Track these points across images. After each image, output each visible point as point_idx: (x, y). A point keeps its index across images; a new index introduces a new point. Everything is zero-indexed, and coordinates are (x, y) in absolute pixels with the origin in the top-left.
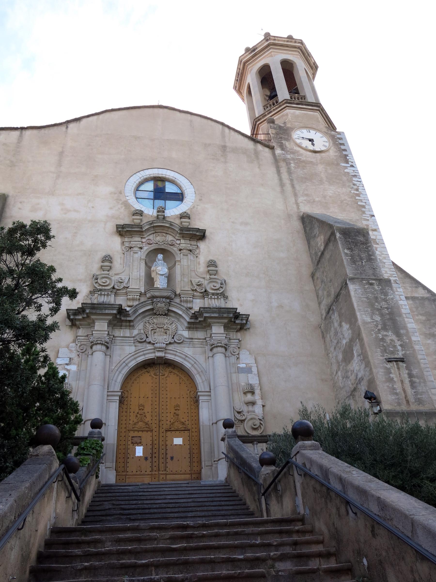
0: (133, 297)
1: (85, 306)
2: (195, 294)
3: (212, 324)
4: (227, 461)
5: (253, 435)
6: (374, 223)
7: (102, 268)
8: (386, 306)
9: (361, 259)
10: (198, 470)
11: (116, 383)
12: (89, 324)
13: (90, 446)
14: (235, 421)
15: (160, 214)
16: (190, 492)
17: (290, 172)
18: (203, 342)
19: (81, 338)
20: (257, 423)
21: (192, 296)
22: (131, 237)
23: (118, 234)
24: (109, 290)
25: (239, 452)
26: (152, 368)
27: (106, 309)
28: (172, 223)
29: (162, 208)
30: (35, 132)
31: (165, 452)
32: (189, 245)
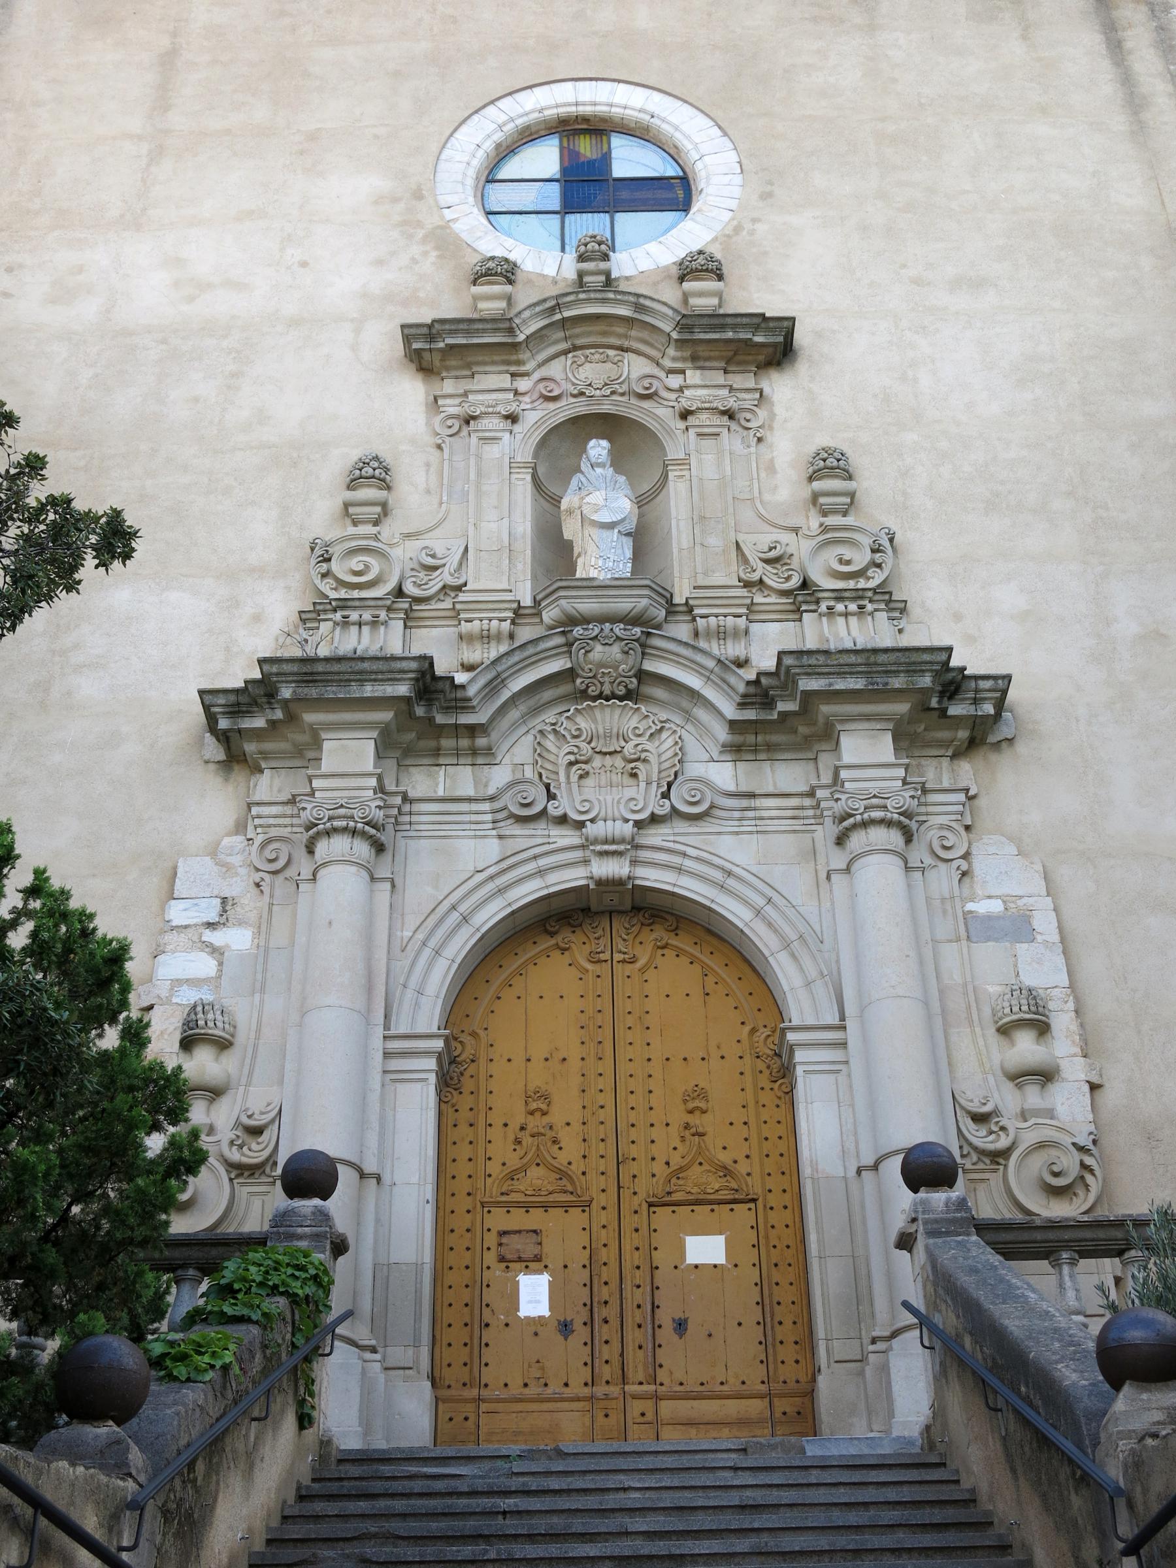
0: (485, 627)
1: (275, 669)
2: (759, 599)
3: (839, 727)
4: (931, 1348)
5: (1050, 1221)
7: (347, 513)
10: (803, 1379)
11: (423, 1000)
12: (299, 752)
13: (259, 1279)
14: (963, 1156)
16: (751, 1496)
18: (802, 808)
19: (266, 810)
20: (1070, 1162)
21: (744, 610)
22: (469, 373)
23: (413, 367)
24: (380, 603)
25: (987, 1305)
26: (578, 930)
27: (363, 677)
28: (642, 301)
31: (649, 1299)
32: (725, 392)
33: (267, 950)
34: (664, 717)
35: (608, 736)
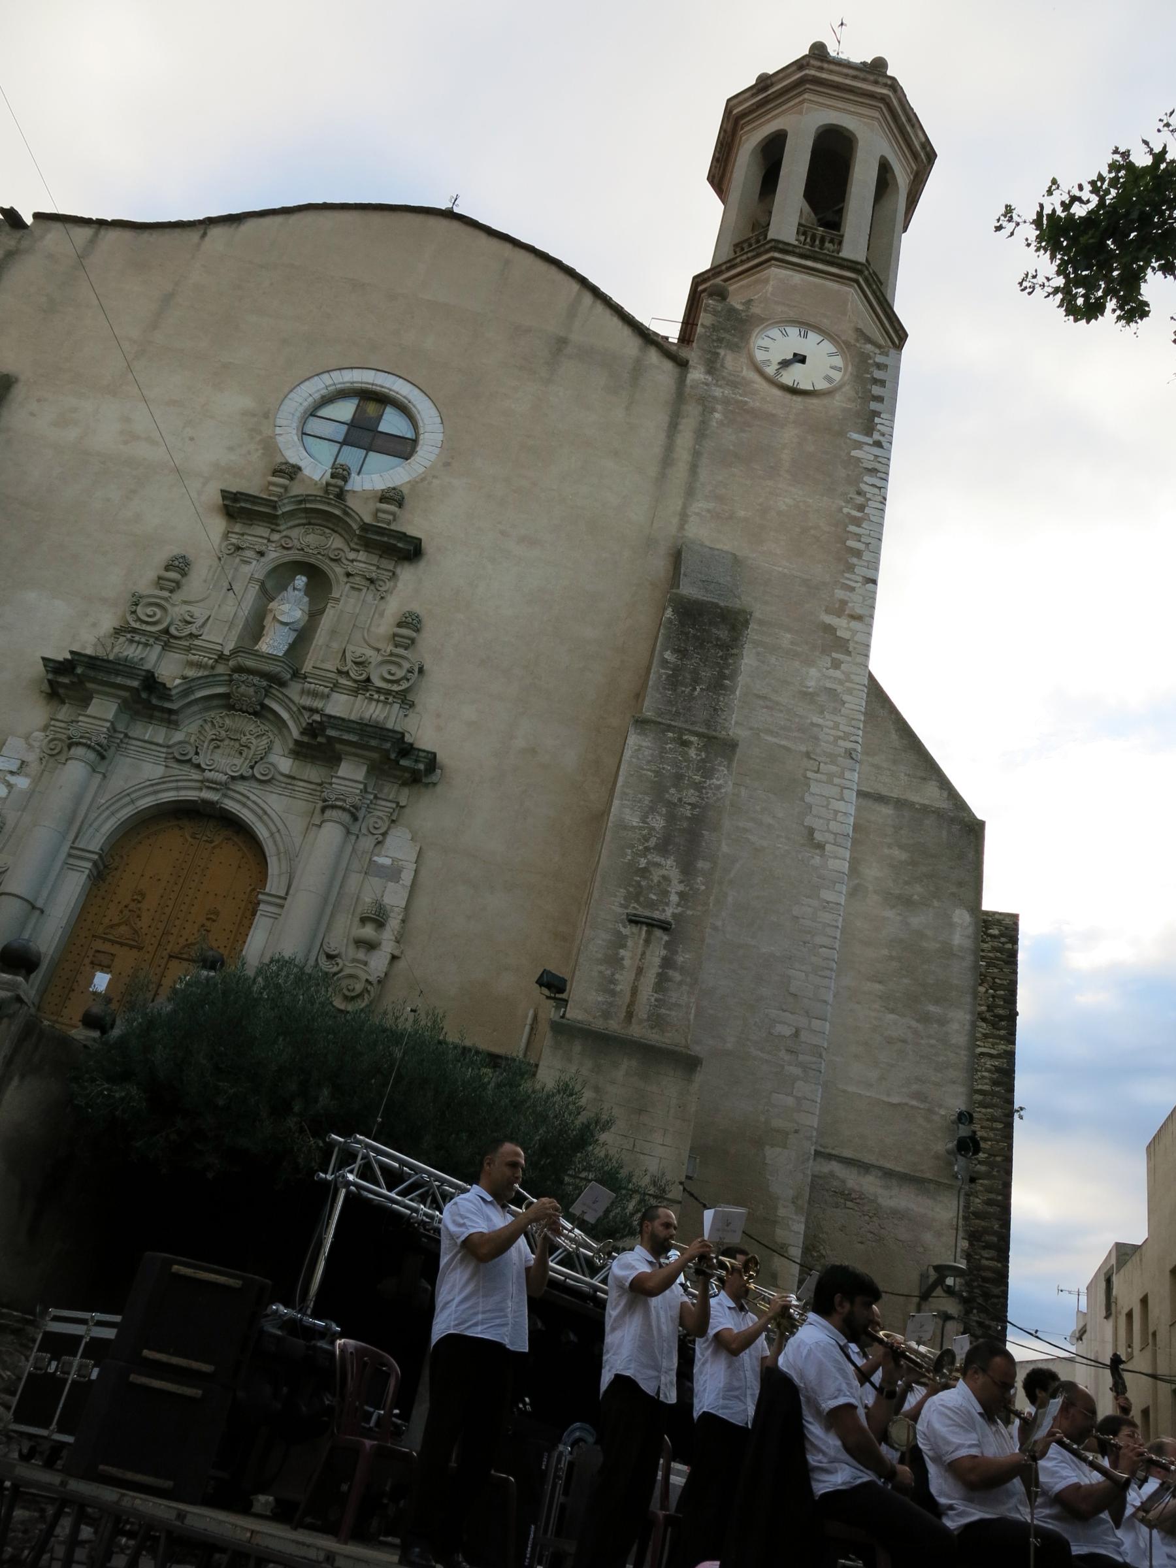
1: (76, 658)
6: (864, 600)
7: (158, 583)
8: (693, 800)
9: (696, 680)
15: (333, 481)
17: (701, 433)
18: (315, 790)
27: (117, 673)
29: (344, 470)
30: (127, 235)
32: (374, 568)
33: (34, 791)
34: (267, 729)
35: (236, 731)
